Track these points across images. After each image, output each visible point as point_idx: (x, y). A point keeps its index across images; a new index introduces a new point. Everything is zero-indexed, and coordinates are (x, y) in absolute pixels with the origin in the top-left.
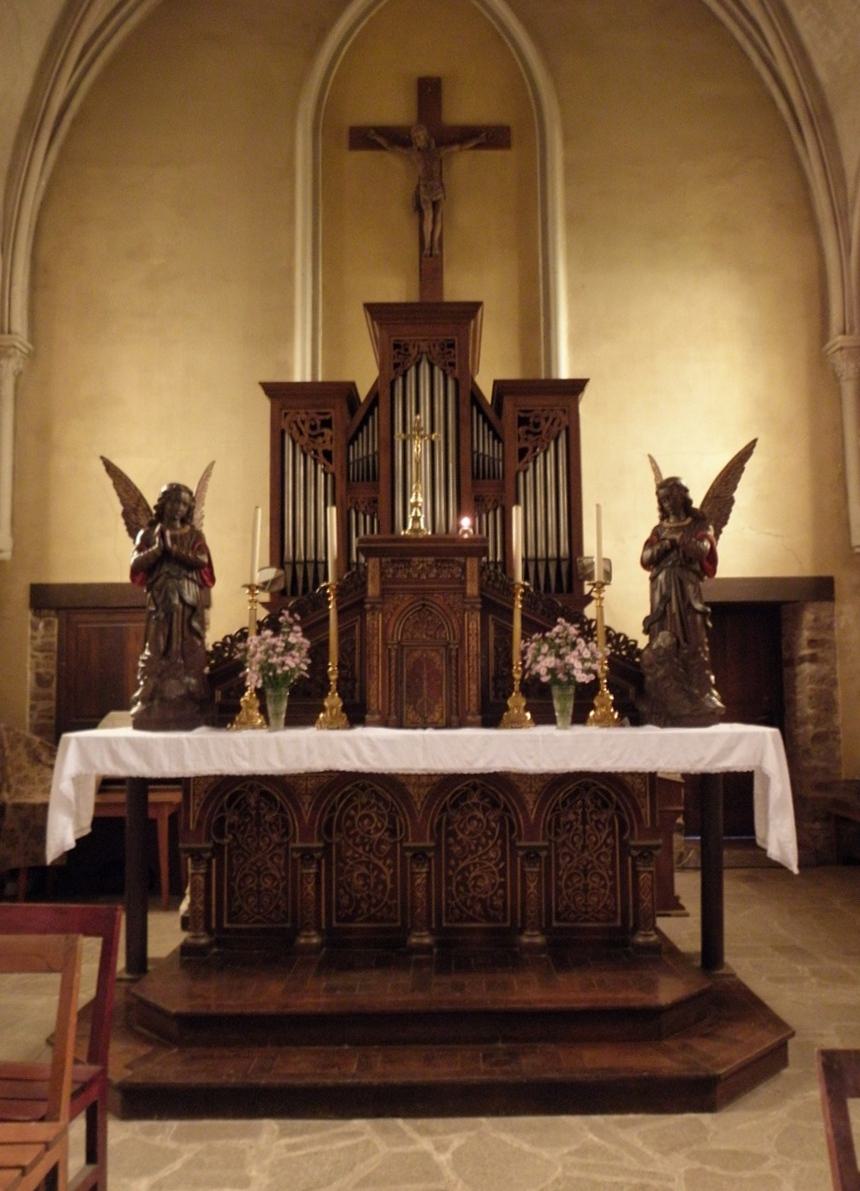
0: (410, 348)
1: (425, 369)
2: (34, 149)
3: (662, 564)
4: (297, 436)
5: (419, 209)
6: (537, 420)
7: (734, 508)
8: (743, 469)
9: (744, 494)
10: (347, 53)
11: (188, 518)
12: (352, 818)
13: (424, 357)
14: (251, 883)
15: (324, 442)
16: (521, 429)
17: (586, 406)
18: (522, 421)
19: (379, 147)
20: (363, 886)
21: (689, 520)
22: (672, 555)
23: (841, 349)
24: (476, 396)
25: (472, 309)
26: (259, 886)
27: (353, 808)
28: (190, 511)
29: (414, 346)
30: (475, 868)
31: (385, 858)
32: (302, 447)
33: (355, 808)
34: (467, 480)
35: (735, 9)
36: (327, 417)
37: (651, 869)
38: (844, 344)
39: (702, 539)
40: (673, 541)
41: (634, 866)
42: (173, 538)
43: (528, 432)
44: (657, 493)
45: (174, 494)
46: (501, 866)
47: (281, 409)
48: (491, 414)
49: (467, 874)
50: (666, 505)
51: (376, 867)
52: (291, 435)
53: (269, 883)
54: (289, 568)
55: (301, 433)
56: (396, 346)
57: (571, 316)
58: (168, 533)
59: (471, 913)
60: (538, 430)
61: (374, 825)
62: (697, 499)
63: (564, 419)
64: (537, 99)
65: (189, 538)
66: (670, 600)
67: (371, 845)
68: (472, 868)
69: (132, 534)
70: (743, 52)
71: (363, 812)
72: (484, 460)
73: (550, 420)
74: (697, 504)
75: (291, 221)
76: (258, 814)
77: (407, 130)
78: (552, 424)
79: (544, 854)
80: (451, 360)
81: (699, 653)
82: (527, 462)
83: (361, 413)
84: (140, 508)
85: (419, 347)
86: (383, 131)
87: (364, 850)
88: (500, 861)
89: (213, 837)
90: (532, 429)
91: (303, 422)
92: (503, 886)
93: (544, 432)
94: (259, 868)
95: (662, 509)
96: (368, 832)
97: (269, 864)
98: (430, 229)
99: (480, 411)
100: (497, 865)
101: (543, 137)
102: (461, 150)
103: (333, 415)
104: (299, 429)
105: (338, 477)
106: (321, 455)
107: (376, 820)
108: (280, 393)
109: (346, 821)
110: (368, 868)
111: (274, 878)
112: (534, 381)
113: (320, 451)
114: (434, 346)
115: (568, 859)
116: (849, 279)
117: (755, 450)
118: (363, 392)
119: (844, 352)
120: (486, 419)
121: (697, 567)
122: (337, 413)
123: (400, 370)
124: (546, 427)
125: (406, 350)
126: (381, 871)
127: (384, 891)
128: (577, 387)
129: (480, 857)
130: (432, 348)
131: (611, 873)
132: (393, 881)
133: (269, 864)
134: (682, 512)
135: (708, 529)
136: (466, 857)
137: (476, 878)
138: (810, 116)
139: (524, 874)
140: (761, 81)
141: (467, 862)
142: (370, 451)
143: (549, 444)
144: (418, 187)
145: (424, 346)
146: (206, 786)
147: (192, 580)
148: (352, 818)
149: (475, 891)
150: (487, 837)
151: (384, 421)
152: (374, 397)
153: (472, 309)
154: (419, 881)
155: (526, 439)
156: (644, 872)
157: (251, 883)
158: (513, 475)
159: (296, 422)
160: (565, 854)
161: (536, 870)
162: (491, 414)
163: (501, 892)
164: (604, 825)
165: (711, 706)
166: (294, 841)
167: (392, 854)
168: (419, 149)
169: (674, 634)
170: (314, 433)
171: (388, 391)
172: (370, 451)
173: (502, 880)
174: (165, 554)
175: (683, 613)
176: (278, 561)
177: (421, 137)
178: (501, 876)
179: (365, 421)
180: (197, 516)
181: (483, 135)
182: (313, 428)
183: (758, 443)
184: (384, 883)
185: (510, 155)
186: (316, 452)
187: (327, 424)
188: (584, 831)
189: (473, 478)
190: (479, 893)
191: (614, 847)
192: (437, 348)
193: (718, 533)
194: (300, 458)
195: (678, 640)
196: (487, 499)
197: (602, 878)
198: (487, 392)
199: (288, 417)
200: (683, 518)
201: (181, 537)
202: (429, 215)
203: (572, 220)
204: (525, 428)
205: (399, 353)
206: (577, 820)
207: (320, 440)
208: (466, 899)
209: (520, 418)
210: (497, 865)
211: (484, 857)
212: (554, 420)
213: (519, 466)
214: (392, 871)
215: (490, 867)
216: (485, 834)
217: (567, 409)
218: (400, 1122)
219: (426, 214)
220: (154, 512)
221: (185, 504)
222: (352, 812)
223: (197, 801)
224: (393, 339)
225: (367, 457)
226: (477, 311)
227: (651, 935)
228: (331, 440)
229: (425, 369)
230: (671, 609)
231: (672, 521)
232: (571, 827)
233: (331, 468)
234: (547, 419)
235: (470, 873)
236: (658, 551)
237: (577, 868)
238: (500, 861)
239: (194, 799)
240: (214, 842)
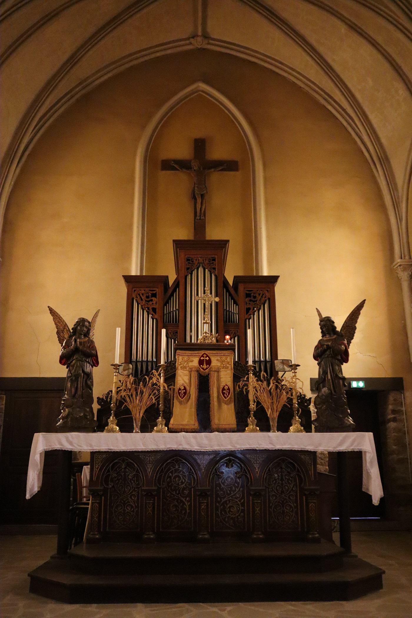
0: (195, 261)
1: (201, 270)
2: (10, 166)
3: (323, 356)
4: (140, 301)
5: (194, 198)
6: (254, 295)
7: (355, 335)
8: (359, 314)
9: (361, 324)
10: (154, 139)
11: (87, 334)
12: (170, 477)
13: (201, 264)
14: (120, 509)
15: (153, 304)
16: (247, 299)
17: (278, 288)
18: (248, 295)
19: (176, 169)
20: (175, 511)
21: (335, 336)
22: (327, 352)
23: (400, 265)
24: (225, 282)
25: (223, 244)
26: (124, 510)
27: (171, 472)
28: (89, 330)
29: (196, 260)
30: (229, 502)
31: (186, 497)
32: (142, 306)
33: (172, 472)
34: (221, 324)
35: (407, 4)
36: (154, 292)
37: (315, 501)
38: (401, 263)
39: (341, 345)
40: (327, 345)
41: (306, 500)
42: (80, 343)
43: (250, 300)
44: (320, 324)
45: (82, 322)
46: (242, 501)
47: (133, 288)
48: (232, 292)
49: (226, 505)
50: (324, 329)
51: (182, 501)
52: (136, 300)
53: (129, 509)
54: (134, 364)
55: (142, 300)
56: (188, 260)
57: (268, 249)
58: (78, 340)
59: (227, 525)
60: (256, 299)
61: (181, 481)
62: (339, 325)
63: (267, 294)
64: (251, 149)
65: (87, 343)
66: (327, 373)
67: (179, 491)
68: (228, 502)
69: (61, 342)
70: (346, 129)
71: (176, 474)
72: (229, 314)
73: (261, 295)
74: (339, 329)
75: (132, 202)
76: (125, 474)
77: (189, 161)
78: (262, 297)
79: (263, 493)
80: (214, 267)
81: (342, 398)
82: (250, 314)
83: (170, 291)
84: (65, 330)
85: (198, 260)
86: (177, 162)
87: (176, 493)
88: (241, 499)
89: (104, 484)
90: (252, 298)
91: (143, 294)
92: (243, 511)
93: (258, 300)
94: (125, 501)
95: (322, 332)
96: (178, 484)
97: (130, 500)
98: (200, 207)
99: (228, 291)
100: (240, 501)
101: (254, 166)
102: (215, 171)
103: (157, 291)
104: (140, 297)
105: (159, 320)
106: (151, 310)
107: (182, 478)
108: (129, 279)
109: (167, 478)
110: (177, 501)
111: (132, 507)
112: (252, 276)
113: (150, 308)
114: (206, 260)
115: (274, 498)
116: (402, 234)
117: (365, 305)
118: (171, 282)
119: (401, 267)
120: (230, 295)
121: (339, 358)
122: (159, 290)
123: (189, 271)
124: (259, 298)
125: (193, 262)
126: (184, 504)
127: (185, 513)
128: (273, 279)
129: (232, 496)
130: (205, 260)
131: (295, 505)
132: (190, 508)
133: (130, 500)
134: (332, 333)
135: (345, 341)
136: (225, 497)
137: (230, 507)
138: (379, 159)
139: (253, 503)
140: (355, 143)
141: (225, 499)
142: (174, 309)
143: (260, 306)
144: (194, 187)
145: (201, 260)
146: (101, 459)
147: (89, 363)
148: (170, 477)
149: (230, 514)
150: (236, 487)
151: (182, 294)
152: (177, 283)
153: (223, 244)
154: (203, 507)
155: (250, 304)
156: (311, 502)
157: (120, 509)
158: (244, 322)
159: (139, 294)
160: (273, 495)
161: (259, 501)
162: (232, 292)
163: (242, 514)
164: (291, 481)
165: (348, 423)
166: (144, 486)
167: (189, 495)
168: (195, 170)
169: (329, 389)
170: (148, 300)
171: (184, 280)
172: (174, 309)
173: (243, 508)
174: (76, 350)
175: (334, 380)
176: (129, 360)
177: (195, 165)
178: (242, 507)
179: (172, 295)
180: (91, 334)
181: (225, 165)
182: (147, 297)
183: (366, 302)
184: (185, 509)
185: (238, 174)
186: (148, 309)
187: (154, 295)
188: (282, 484)
189: (224, 322)
190: (232, 515)
191: (296, 492)
192: (207, 262)
193: (349, 343)
194: (140, 311)
195: (331, 391)
196: (231, 332)
197: (291, 507)
198: (231, 282)
199: (136, 292)
200: (332, 335)
201: (84, 342)
202: (199, 201)
203: (267, 203)
204: (249, 299)
205: (189, 263)
206: (278, 478)
207: (151, 303)
208: (225, 518)
209: (225, 332)
210: (240, 501)
211: (234, 497)
212: (263, 295)
213: (246, 316)
214: (189, 503)
215: (237, 502)
216: (234, 485)
217: (269, 289)
218: (240, 603)
219: (198, 201)
220: (72, 331)
221: (86, 327)
222: (171, 474)
223: (96, 467)
224: (186, 256)
225: (173, 312)
226: (226, 244)
227: (316, 534)
228: (156, 303)
229: (201, 270)
230: (328, 377)
231: (327, 337)
232: (276, 482)
233: (156, 316)
234: (259, 294)
235: (227, 505)
236: (321, 351)
237: (279, 502)
238: (241, 499)
239: (96, 465)
240: (104, 487)
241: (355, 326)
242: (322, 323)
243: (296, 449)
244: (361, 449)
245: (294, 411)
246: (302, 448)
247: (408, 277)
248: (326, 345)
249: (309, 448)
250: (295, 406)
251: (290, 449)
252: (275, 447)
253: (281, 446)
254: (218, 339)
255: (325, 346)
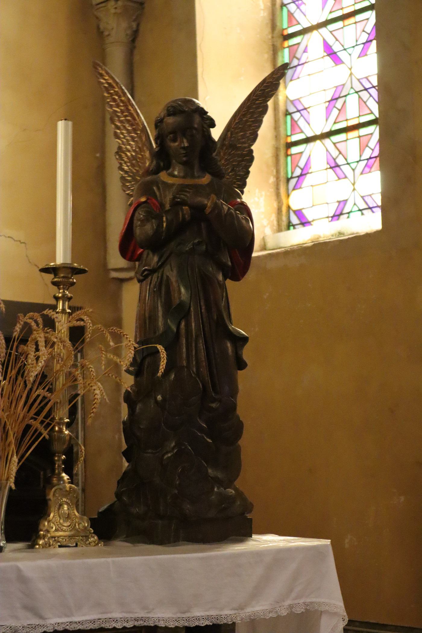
241: (252, 151)
242: (170, 120)
243: (119, 626)
244: (312, 603)
245: (54, 455)
246: (136, 620)
247: (127, 35)
248: (192, 207)
249: (160, 615)
250: (61, 431)
251: (96, 626)
252: (41, 622)
253: (67, 616)
254: (165, 120)
255: (185, 208)
